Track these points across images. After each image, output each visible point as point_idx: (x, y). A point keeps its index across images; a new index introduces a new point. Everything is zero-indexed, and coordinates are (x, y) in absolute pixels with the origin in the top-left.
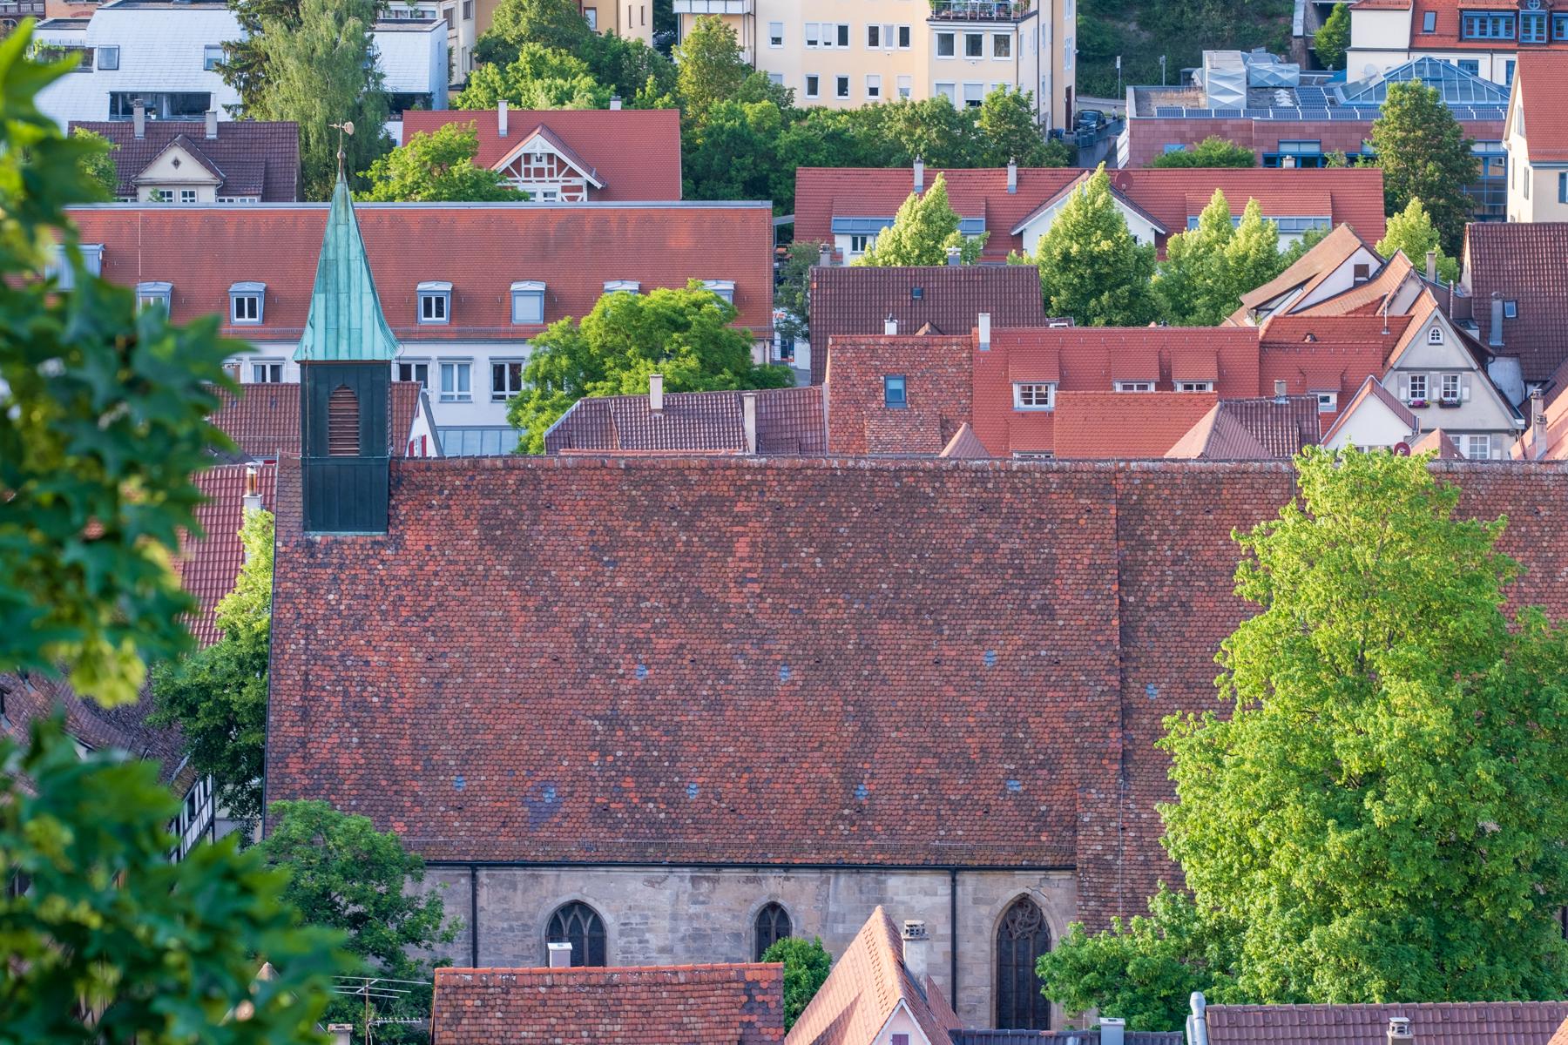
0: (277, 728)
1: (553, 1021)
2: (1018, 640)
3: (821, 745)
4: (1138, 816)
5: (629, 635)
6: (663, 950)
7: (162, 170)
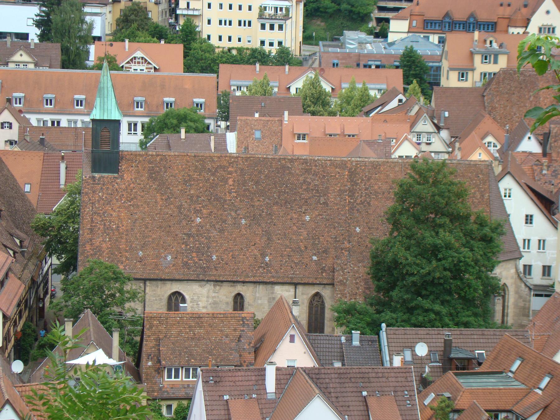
0: (83, 235)
1: (182, 328)
2: (317, 213)
3: (255, 244)
4: (353, 268)
5: (195, 208)
6: (204, 307)
7: (17, 57)
